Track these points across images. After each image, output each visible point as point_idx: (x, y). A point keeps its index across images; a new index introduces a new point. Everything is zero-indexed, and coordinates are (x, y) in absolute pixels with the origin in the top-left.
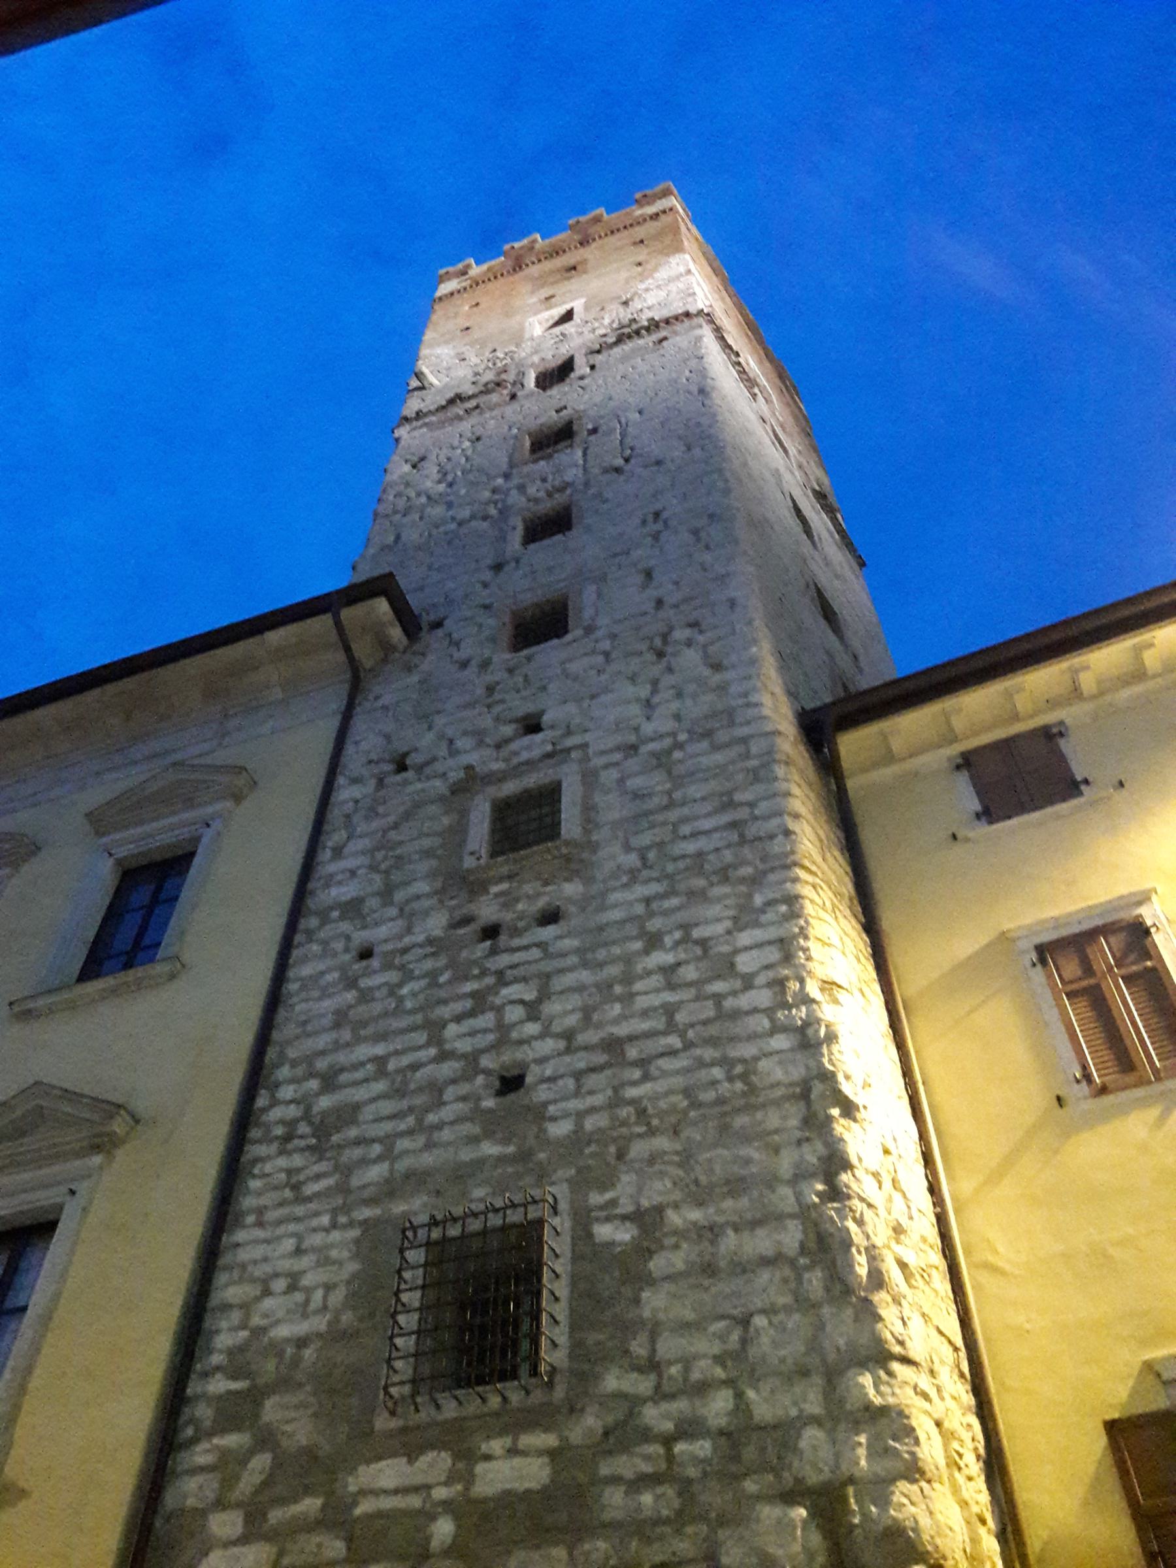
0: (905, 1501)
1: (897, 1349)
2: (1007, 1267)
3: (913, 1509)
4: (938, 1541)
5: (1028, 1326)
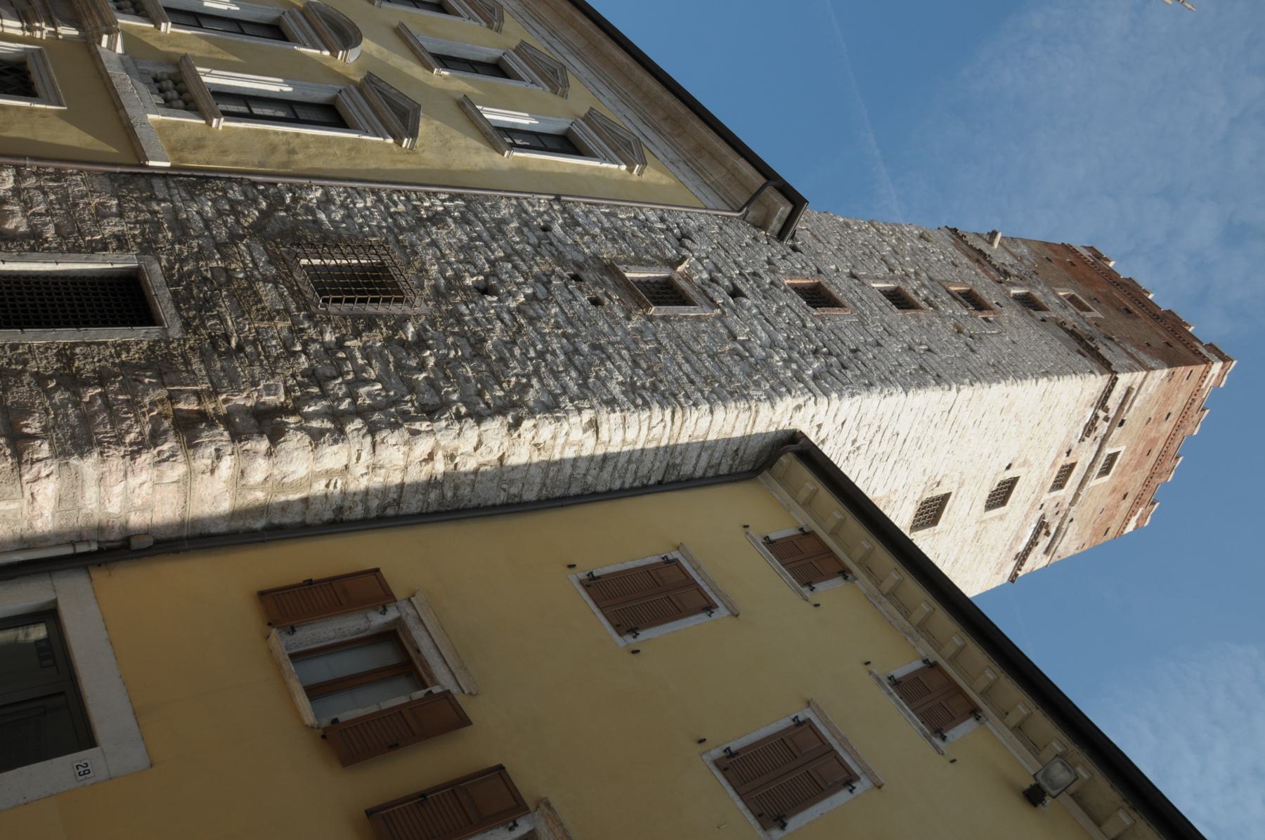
1: (378, 438)
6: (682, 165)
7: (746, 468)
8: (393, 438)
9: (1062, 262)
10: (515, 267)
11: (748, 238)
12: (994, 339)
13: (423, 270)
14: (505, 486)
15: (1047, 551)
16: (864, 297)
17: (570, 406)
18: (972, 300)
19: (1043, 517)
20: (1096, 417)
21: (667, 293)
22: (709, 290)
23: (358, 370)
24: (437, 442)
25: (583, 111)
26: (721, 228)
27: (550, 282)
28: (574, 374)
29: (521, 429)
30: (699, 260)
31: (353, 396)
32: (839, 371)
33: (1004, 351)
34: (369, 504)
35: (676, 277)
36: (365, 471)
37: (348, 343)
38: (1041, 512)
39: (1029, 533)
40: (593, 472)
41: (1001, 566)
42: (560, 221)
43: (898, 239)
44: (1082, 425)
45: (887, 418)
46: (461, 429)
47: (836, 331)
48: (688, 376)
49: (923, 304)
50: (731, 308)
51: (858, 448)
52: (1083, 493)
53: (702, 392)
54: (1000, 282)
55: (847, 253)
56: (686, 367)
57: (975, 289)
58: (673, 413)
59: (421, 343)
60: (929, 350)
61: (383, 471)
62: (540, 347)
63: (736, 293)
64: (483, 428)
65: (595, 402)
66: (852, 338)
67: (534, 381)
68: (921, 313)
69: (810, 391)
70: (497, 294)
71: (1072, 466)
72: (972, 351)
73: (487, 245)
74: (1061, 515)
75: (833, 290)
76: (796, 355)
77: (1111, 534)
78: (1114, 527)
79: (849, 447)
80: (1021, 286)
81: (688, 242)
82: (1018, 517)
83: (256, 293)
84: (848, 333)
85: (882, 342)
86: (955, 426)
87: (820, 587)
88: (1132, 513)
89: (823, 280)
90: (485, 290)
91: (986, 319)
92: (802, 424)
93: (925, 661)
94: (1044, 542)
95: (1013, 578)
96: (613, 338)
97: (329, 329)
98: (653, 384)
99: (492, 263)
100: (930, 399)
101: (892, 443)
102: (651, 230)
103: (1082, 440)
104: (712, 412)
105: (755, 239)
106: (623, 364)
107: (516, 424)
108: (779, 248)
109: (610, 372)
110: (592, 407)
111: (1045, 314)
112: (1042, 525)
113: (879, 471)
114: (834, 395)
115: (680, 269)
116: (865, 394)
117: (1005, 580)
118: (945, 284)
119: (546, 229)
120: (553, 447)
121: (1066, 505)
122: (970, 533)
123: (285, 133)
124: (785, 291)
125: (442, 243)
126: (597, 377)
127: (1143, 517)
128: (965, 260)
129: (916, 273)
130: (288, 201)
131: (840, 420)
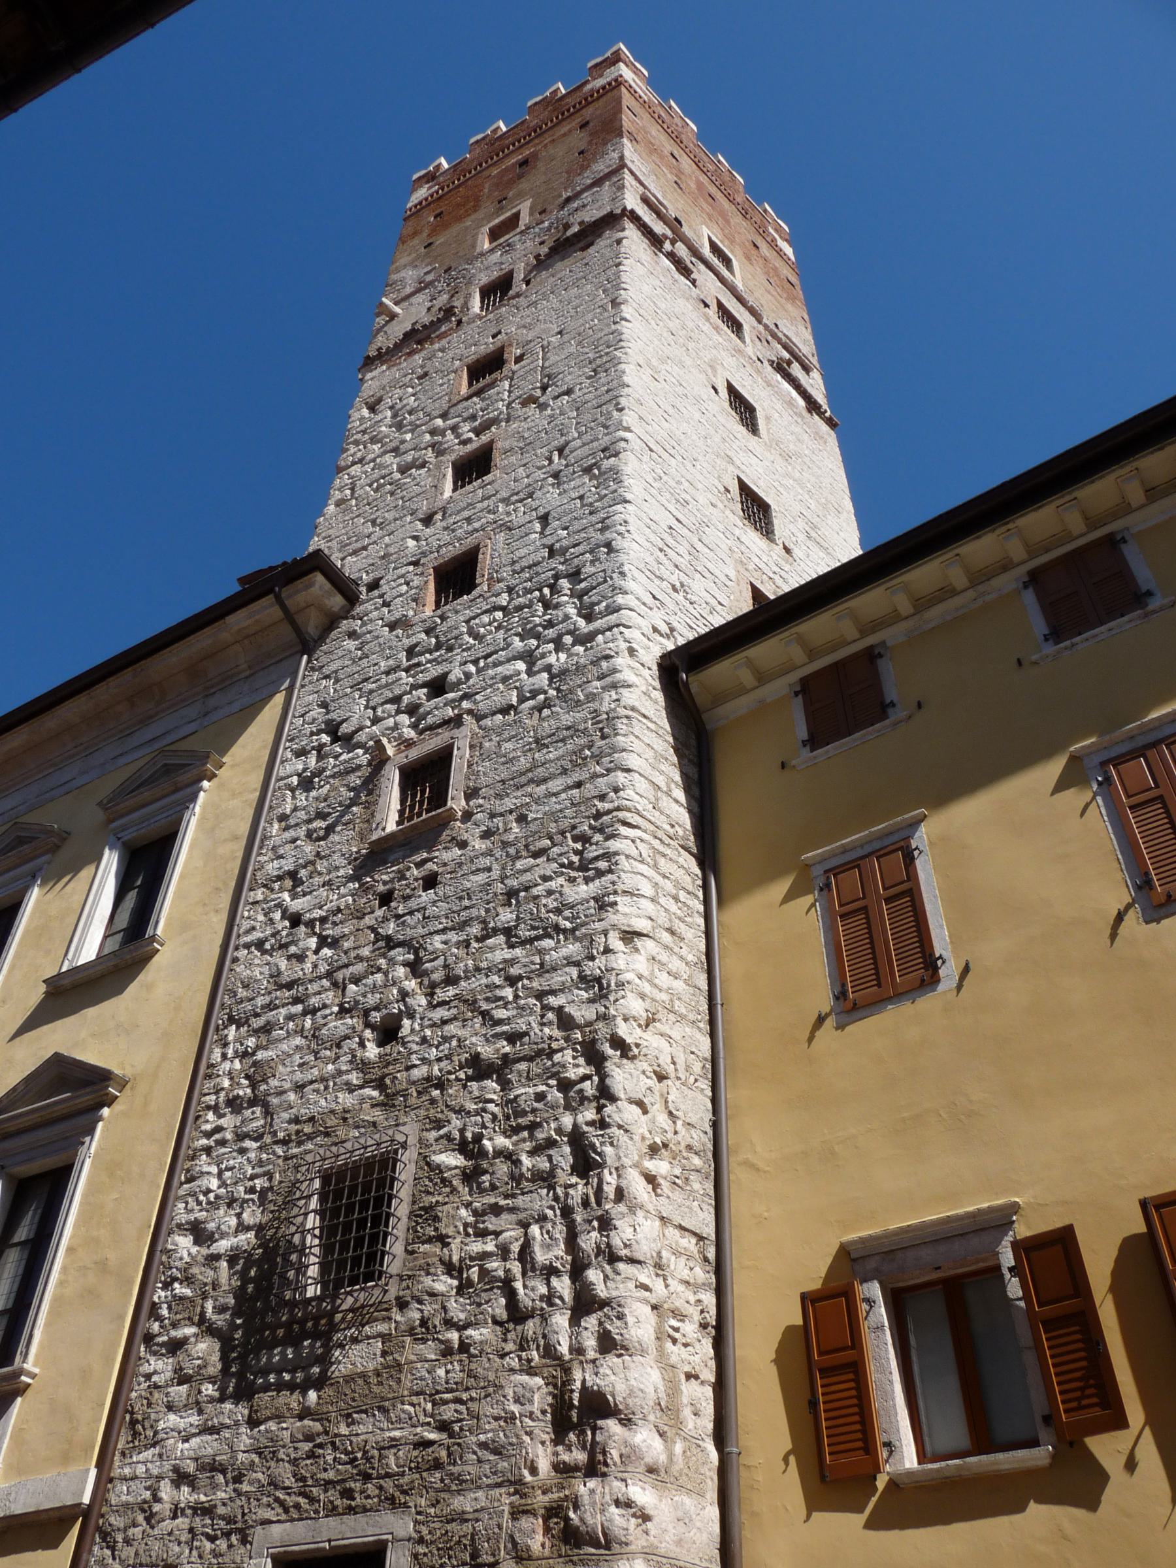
0: (608, 1372)
1: (624, 1252)
2: (761, 1165)
3: (613, 1378)
4: (630, 1401)
5: (766, 1214)
6: (212, 702)
7: (693, 742)
8: (623, 1233)
9: (434, 231)
10: (356, 980)
11: (351, 644)
12: (553, 358)
13: (344, 1117)
14: (692, 1080)
15: (806, 369)
16: (466, 514)
17: (601, 962)
18: (486, 368)
19: (771, 363)
20: (671, 256)
21: (428, 776)
22: (430, 720)
23: (504, 1252)
24: (636, 1165)
25: (100, 816)
26: (327, 677)
27: (388, 939)
28: (548, 943)
29: (629, 1040)
30: (376, 721)
31: (550, 1272)
32: (581, 579)
33: (573, 349)
34: (700, 1282)
35: (402, 759)
36: (661, 1280)
37: (455, 1258)
38: (766, 363)
39: (786, 386)
40: (684, 952)
41: (817, 436)
42: (286, 896)
43: (373, 440)
44: (677, 275)
45: (653, 537)
46: (620, 1127)
47: (517, 567)
48: (570, 788)
49: (485, 438)
50: (463, 698)
51: (682, 585)
52: (751, 302)
53: (596, 775)
54: (459, 322)
55: (389, 516)
56: (555, 785)
57: (469, 360)
58: (625, 824)
59: (470, 1148)
60: (561, 451)
61: (664, 1254)
62: (496, 979)
63: (438, 687)
64: (622, 1096)
65: (598, 926)
66: (532, 547)
67: (553, 1001)
68: (499, 444)
69: (610, 629)
70: (398, 1018)
71: (720, 305)
72: (569, 392)
73: (314, 1011)
74: (770, 338)
75: (448, 553)
76: (551, 633)
77: (794, 279)
78: (786, 272)
79: (680, 597)
80: (468, 297)
81: (345, 729)
82: (771, 398)
83: (349, 1379)
84: (523, 552)
85: (541, 511)
86: (667, 447)
87: (891, 693)
88: (772, 244)
89: (431, 562)
90: (388, 1033)
91: (519, 359)
92: (653, 652)
93: (1026, 586)
94: (796, 370)
95: (831, 423)
96: (496, 873)
97: (428, 1281)
98: (575, 839)
99: (343, 1011)
100: (633, 468)
101: (680, 539)
102: (319, 773)
103: (694, 282)
104: (628, 771)
105: (352, 635)
106: (539, 871)
107: (619, 1043)
108: (367, 605)
109: (550, 893)
110: (605, 933)
111: (519, 276)
112: (781, 368)
113: (709, 565)
114: (620, 599)
115: (390, 751)
116: (622, 557)
117: (832, 432)
118: (455, 399)
119: (295, 920)
120: (653, 1000)
121: (761, 328)
122: (780, 464)
123: (64, 1269)
124: (443, 618)
125: (299, 1077)
126: (558, 911)
127: (778, 230)
128: (418, 359)
129: (433, 432)
130: (188, 1292)
131: (649, 600)
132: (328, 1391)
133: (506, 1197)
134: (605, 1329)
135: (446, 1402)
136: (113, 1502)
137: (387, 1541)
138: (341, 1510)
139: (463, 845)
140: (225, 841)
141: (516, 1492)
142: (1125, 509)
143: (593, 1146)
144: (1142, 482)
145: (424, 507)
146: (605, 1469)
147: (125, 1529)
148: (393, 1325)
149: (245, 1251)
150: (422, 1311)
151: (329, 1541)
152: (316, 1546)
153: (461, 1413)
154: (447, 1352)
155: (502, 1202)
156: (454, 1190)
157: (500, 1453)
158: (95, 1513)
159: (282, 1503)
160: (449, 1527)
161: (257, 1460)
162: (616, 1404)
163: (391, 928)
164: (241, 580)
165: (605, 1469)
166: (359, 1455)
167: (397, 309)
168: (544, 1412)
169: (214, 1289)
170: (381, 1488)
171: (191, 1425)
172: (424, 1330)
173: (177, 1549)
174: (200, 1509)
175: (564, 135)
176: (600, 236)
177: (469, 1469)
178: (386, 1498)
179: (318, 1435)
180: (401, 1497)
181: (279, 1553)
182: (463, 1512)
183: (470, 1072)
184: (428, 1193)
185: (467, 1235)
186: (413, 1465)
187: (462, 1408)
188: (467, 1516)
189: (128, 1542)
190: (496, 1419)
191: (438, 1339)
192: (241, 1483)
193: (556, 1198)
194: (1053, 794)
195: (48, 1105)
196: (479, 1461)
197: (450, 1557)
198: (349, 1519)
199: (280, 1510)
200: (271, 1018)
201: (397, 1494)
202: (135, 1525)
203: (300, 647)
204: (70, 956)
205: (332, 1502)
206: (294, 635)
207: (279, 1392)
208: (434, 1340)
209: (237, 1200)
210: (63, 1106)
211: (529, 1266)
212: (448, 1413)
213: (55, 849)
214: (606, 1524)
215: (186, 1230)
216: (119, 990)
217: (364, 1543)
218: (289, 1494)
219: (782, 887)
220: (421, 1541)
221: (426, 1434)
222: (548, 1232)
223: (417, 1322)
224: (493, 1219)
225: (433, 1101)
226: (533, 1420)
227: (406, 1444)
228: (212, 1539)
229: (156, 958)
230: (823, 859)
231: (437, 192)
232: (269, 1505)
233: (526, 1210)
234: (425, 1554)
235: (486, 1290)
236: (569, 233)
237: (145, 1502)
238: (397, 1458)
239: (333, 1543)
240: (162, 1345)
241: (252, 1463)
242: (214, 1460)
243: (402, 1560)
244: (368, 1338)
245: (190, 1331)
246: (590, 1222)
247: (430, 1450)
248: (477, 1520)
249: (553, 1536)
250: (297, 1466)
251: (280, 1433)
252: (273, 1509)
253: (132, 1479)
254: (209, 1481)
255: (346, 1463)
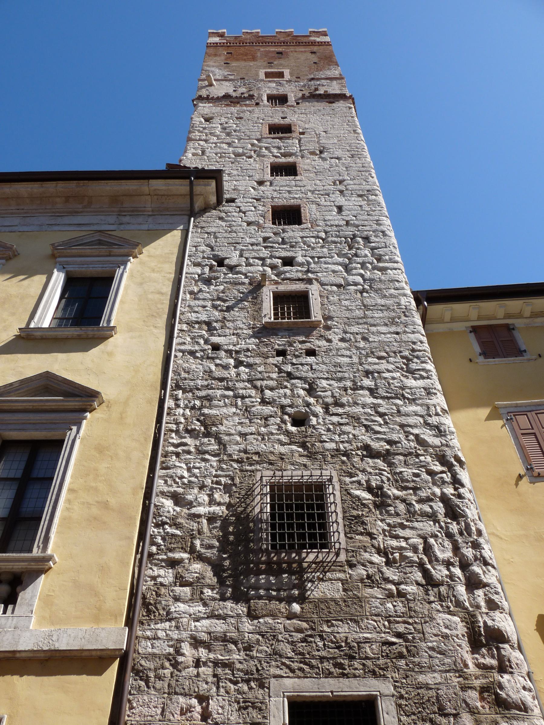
2: (503, 537)
31: (448, 564)
69: (396, 269)
97: (367, 555)
132: (306, 606)
133: (407, 521)
134: (490, 598)
135: (398, 622)
136: (140, 651)
137: (376, 695)
138: (335, 675)
139: (329, 341)
140: (152, 292)
141: (460, 676)
142: (520, 315)
143: (458, 506)
144: (451, 314)
145: (257, 177)
146: (511, 670)
147: (156, 670)
148: (348, 576)
149: (221, 516)
150: (367, 571)
151: (332, 692)
152: (322, 694)
153: (410, 630)
154: (390, 595)
155: (406, 523)
156: (370, 510)
157: (444, 654)
158: (132, 655)
159: (288, 667)
160: (419, 691)
161: (261, 638)
162: (508, 637)
163: (289, 368)
164: (168, 165)
165: (511, 670)
166: (343, 644)
167: (214, 83)
168: (463, 636)
169: (199, 534)
170: (364, 665)
171: (199, 612)
172: (370, 581)
173: (205, 686)
174: (220, 663)
175: (302, 52)
176: (338, 101)
177: (425, 660)
178: (369, 671)
179: (306, 629)
180: (380, 671)
181: (293, 696)
182: (427, 684)
183: (365, 453)
184: (354, 509)
185: (385, 536)
186: (384, 654)
187: (411, 627)
188: (431, 686)
189: (159, 678)
190: (436, 635)
191: (381, 587)
192: (252, 651)
193: (441, 527)
194: (486, 420)
195: (35, 401)
196: (430, 657)
197: (424, 708)
198: (345, 681)
199: (287, 671)
200: (210, 393)
201: (377, 669)
202: (163, 667)
203: (189, 213)
204: (36, 319)
205: (328, 670)
206: (189, 205)
207: (270, 601)
208: (378, 587)
209: (206, 486)
210: (54, 404)
211: (433, 559)
212: (401, 628)
213: (8, 259)
214: (523, 699)
215: (168, 496)
216: (86, 349)
217: (359, 695)
218: (293, 662)
219: (485, 412)
220: (401, 697)
221: (389, 638)
222: (441, 544)
223: (365, 577)
224: (401, 530)
225: (343, 462)
226: (458, 639)
227: (376, 642)
228: (235, 683)
229: (111, 340)
230: (506, 407)
231: (224, 43)
232: (278, 667)
233: (422, 530)
234: (406, 705)
235: (408, 567)
236: (317, 92)
237: (170, 654)
238: (372, 649)
239: (335, 693)
240: (162, 560)
241: (258, 640)
242: (225, 636)
243: (390, 707)
244: (331, 580)
245: (185, 556)
246: (467, 543)
247: (394, 647)
248: (438, 689)
249: (489, 702)
250: (295, 646)
251: (277, 625)
252: (281, 669)
253: (154, 639)
254: (223, 648)
255: (334, 648)
